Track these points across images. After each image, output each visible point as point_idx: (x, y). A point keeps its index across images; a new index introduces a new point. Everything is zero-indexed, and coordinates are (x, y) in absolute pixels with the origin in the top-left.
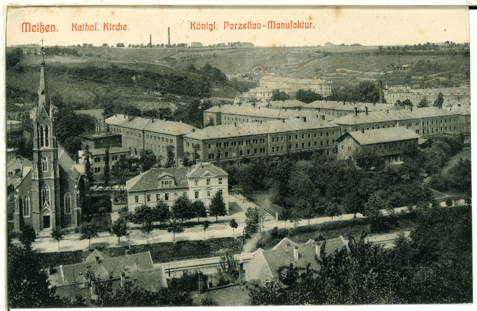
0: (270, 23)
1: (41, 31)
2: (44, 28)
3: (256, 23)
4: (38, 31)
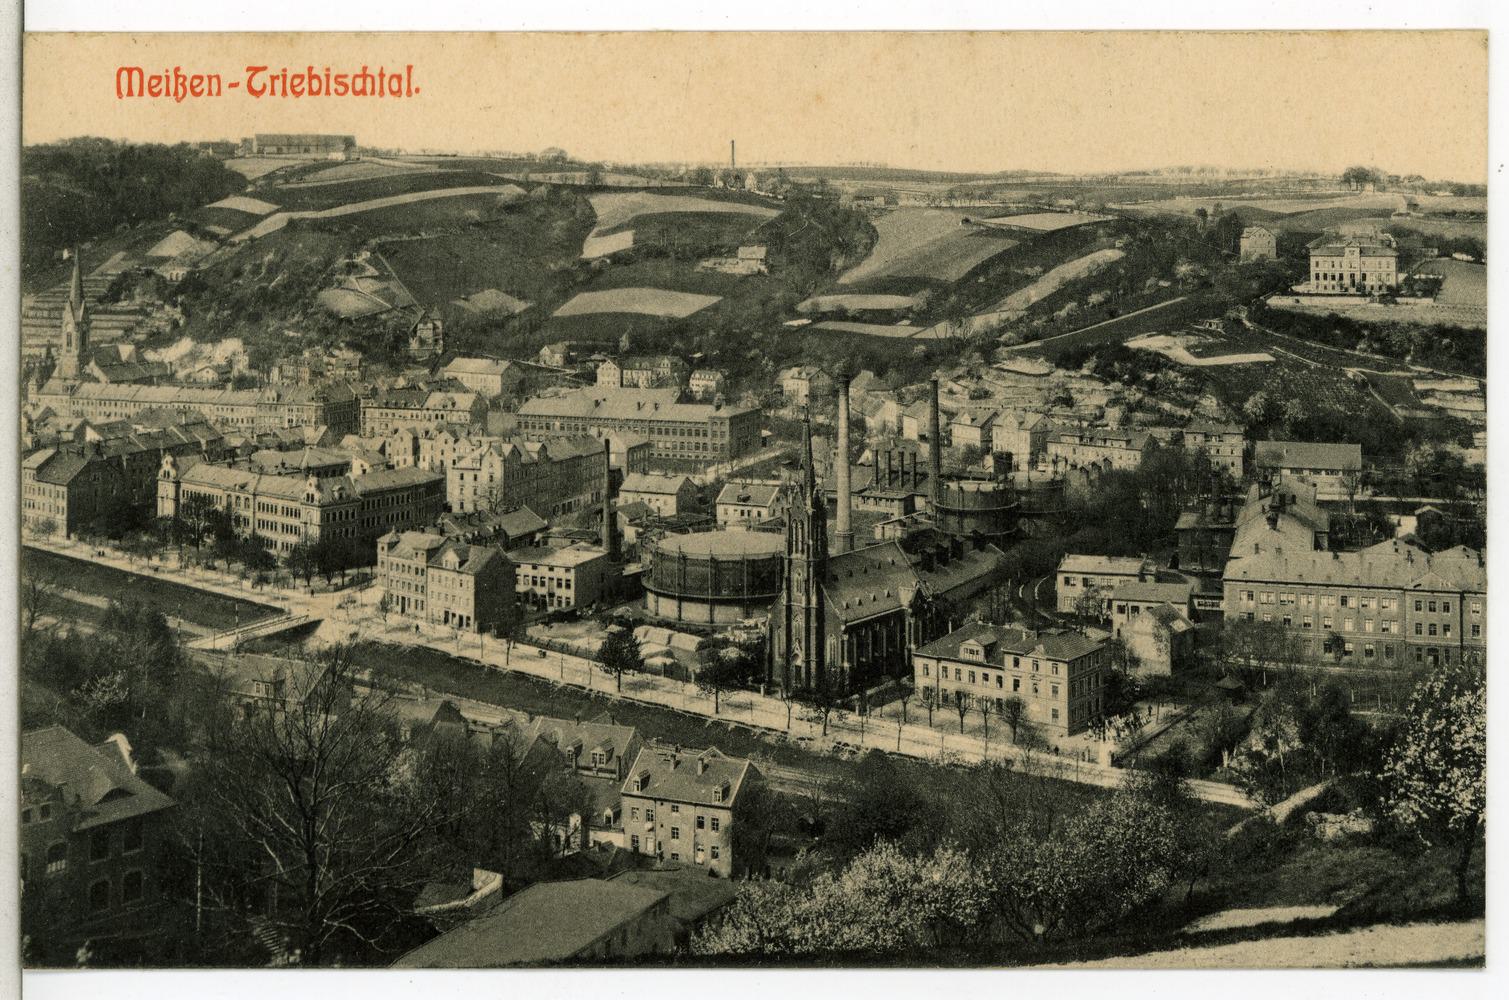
0: (125, 74)
1: (176, 93)
2: (187, 84)
3: (204, 74)
4: (168, 94)
